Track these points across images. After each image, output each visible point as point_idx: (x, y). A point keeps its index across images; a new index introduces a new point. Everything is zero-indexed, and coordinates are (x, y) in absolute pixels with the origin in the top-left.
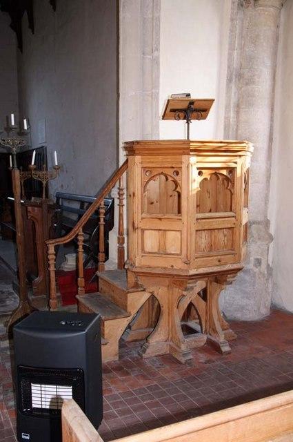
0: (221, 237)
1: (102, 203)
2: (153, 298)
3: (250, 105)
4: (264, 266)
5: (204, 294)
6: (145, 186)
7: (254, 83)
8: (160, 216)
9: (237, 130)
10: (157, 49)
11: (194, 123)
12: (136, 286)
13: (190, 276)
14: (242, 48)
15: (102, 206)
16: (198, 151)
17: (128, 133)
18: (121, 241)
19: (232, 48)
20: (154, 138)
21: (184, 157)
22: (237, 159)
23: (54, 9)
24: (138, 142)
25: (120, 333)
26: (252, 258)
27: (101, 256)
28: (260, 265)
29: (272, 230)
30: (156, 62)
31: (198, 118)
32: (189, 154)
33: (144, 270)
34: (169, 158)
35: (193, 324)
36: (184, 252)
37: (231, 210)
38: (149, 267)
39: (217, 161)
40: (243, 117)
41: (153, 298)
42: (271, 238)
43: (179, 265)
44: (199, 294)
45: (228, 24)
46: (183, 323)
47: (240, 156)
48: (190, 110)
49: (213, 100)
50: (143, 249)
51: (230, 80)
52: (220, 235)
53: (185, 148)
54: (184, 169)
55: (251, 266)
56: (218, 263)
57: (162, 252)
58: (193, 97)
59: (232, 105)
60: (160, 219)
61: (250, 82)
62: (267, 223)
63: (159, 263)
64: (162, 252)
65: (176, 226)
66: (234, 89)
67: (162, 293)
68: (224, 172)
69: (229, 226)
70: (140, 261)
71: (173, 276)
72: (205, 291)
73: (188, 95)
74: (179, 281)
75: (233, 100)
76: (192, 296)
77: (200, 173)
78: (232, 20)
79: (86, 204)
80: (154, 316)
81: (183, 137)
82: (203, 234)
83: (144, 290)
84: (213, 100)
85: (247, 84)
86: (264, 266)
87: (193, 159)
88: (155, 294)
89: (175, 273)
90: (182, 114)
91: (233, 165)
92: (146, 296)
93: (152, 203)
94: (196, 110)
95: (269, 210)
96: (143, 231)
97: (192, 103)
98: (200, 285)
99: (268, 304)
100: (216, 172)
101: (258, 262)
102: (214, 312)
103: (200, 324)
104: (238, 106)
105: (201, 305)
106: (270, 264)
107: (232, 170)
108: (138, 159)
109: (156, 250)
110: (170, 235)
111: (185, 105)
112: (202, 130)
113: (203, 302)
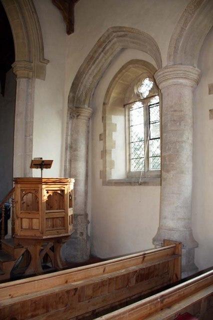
0: (58, 221)
1: (3, 205)
2: (27, 251)
3: (76, 160)
4: (85, 236)
5: (53, 249)
6: (22, 199)
7: (77, 151)
8: (29, 212)
9: (70, 171)
10: (32, 135)
11: (44, 170)
12: (19, 245)
13: (43, 239)
14: (72, 135)
15: (4, 207)
16: (46, 183)
17: (17, 174)
18: (13, 224)
19: (67, 135)
20: (30, 176)
21: (40, 185)
22: (65, 186)
23: (3, 96)
24: (19, 178)
25: (11, 269)
26: (78, 232)
27: (3, 232)
28: (83, 235)
29: (89, 218)
30: (31, 140)
31: (46, 168)
32: (41, 184)
33: (22, 237)
34: (33, 186)
35: (49, 264)
36: (41, 228)
37: (63, 209)
38: (24, 236)
39: (56, 187)
40: (73, 166)
41: (27, 251)
42: (88, 222)
43: (38, 234)
44: (50, 249)
45: (65, 125)
46: (43, 264)
47: (66, 185)
48: (44, 164)
49: (52, 161)
50: (22, 228)
51: (66, 149)
52: (58, 221)
53: (39, 181)
54: (40, 190)
55: (78, 235)
56: (57, 233)
57: (31, 228)
58: (43, 159)
59: (68, 160)
60: (29, 213)
61: (76, 150)
62: (86, 215)
63: (29, 234)
64: (31, 228)
65: (37, 216)
66: (68, 153)
67: (31, 249)
68: (59, 192)
69: (62, 216)
70: (19, 233)
71: (36, 239)
72: (53, 247)
73: (41, 158)
74: (38, 241)
75: (68, 158)
76: (47, 250)
77: (48, 193)
78: (67, 123)
79: (56, 205)
80: (76, 283)
81: (40, 176)
82: (50, 220)
83: (23, 247)
84: (52, 161)
85: (74, 151)
86: (85, 236)
87: (44, 186)
88: (28, 249)
89: (36, 238)
90: (39, 166)
91: (63, 189)
92: (23, 250)
93: (28, 206)
94: (45, 165)
95: (88, 210)
96: (21, 219)
97: (43, 161)
98: (51, 244)
99: (88, 254)
100: (55, 192)
101: (82, 234)
102: (58, 258)
103: (52, 264)
104: (70, 161)
105: (51, 254)
106: (89, 235)
107: (63, 191)
108: (19, 186)
109: (27, 228)
110: (35, 221)
111: (40, 163)
112: (47, 174)
113: (52, 253)
